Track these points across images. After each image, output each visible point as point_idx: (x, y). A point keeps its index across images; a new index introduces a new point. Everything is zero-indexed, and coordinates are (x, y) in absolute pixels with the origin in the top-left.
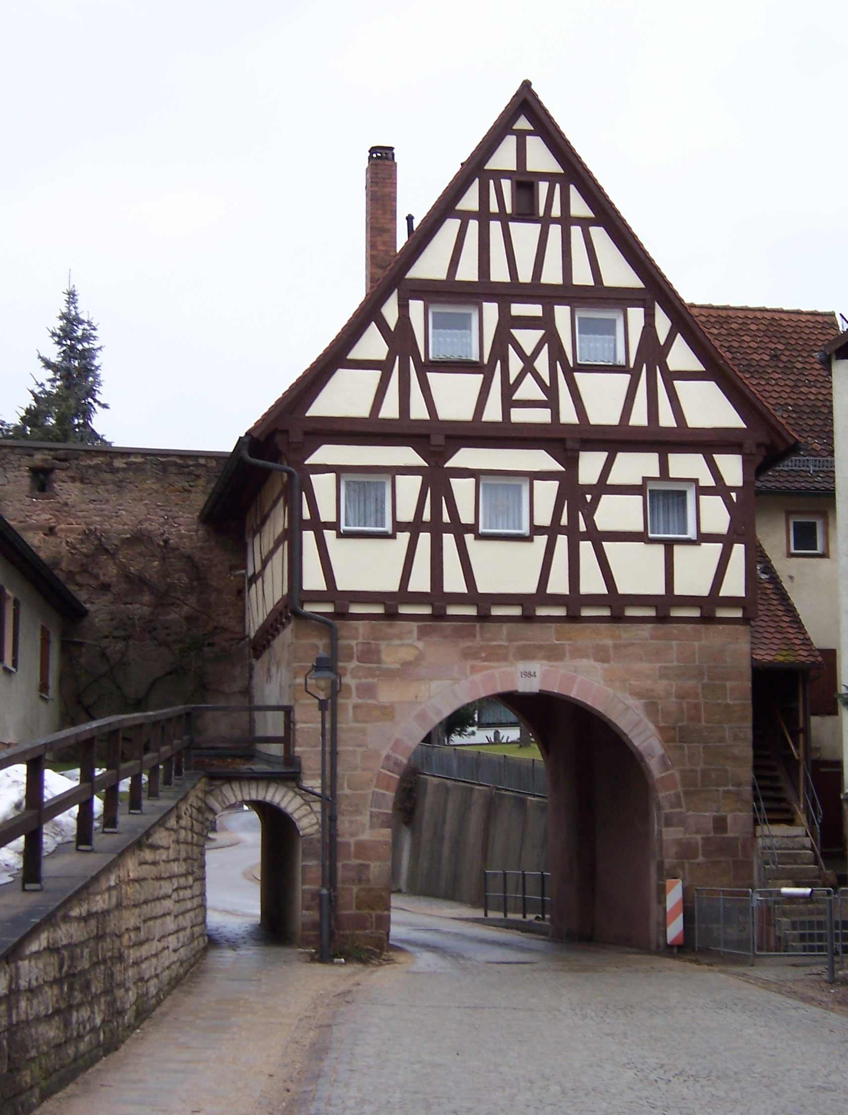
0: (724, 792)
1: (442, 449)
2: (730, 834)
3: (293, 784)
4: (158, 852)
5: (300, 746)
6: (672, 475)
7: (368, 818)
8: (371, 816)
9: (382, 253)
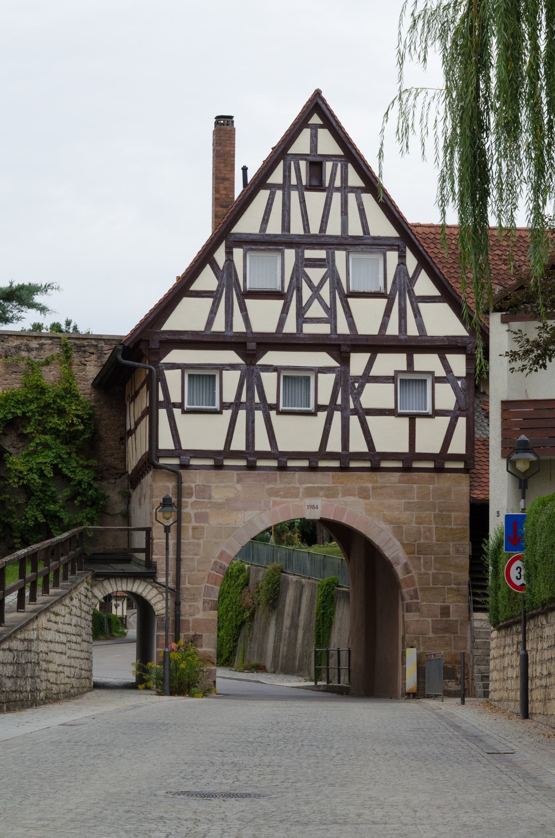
0: (448, 589)
1: (255, 352)
2: (452, 618)
3: (152, 581)
4: (58, 617)
5: (156, 555)
6: (416, 369)
7: (201, 603)
8: (204, 603)
9: (223, 197)
